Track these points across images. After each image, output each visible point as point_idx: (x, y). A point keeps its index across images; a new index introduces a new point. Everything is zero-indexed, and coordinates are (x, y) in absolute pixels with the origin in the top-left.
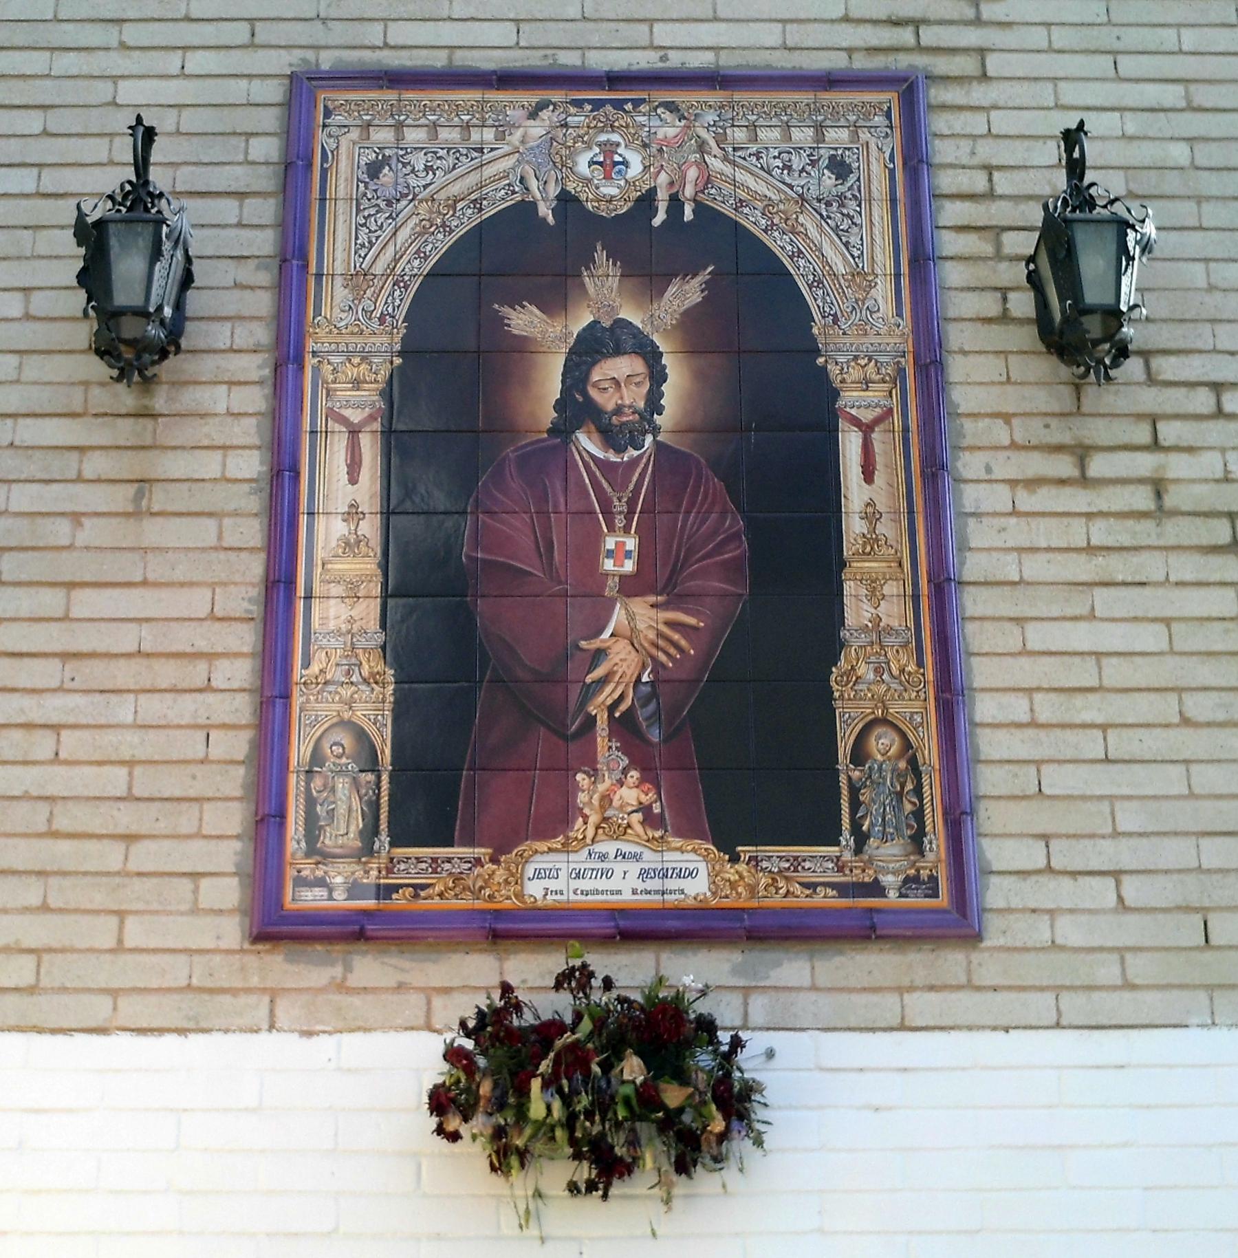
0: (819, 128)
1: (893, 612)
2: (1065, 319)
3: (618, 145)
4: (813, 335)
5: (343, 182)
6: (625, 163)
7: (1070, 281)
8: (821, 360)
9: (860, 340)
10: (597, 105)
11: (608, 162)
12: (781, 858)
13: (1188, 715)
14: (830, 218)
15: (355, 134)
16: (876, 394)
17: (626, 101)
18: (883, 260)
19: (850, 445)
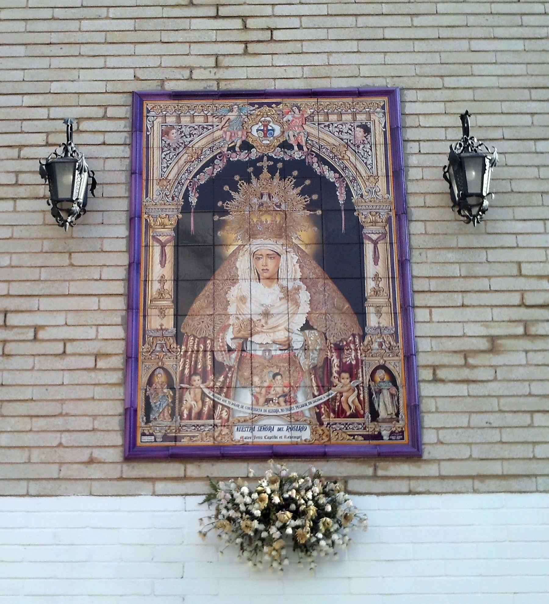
0: (354, 114)
1: (386, 321)
2: (460, 199)
3: (269, 122)
4: (353, 203)
5: (156, 140)
6: (273, 130)
7: (463, 184)
8: (356, 214)
9: (370, 193)
10: (261, 105)
11: (265, 129)
12: (340, 423)
13: (489, 260)
14: (358, 152)
15: (160, 120)
16: (378, 228)
17: (273, 103)
18: (382, 171)
19: (369, 248)
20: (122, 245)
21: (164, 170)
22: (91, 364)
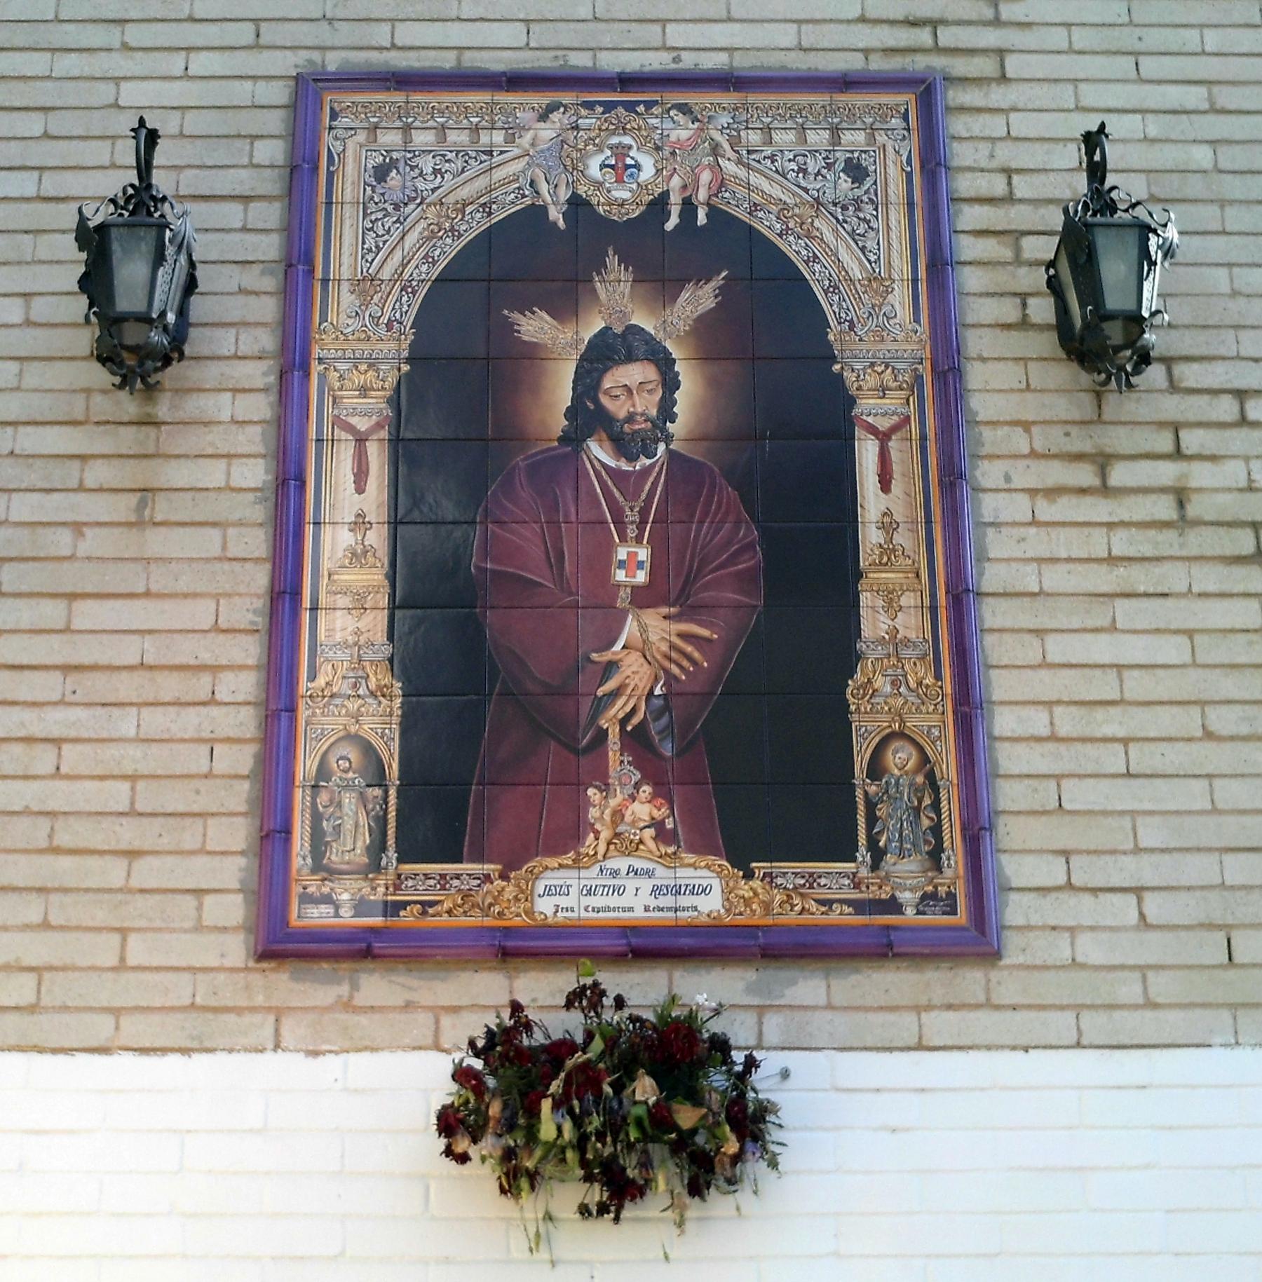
0: (835, 131)
1: (910, 624)
2: (1086, 325)
3: (630, 147)
4: (828, 341)
5: (349, 186)
6: (637, 166)
7: (1091, 287)
8: (837, 367)
9: (876, 346)
10: (609, 107)
11: (620, 165)
12: (796, 874)
14: (846, 222)
16: (893, 402)
17: (638, 103)
18: (900, 265)
19: (867, 453)
22: (249, 38)
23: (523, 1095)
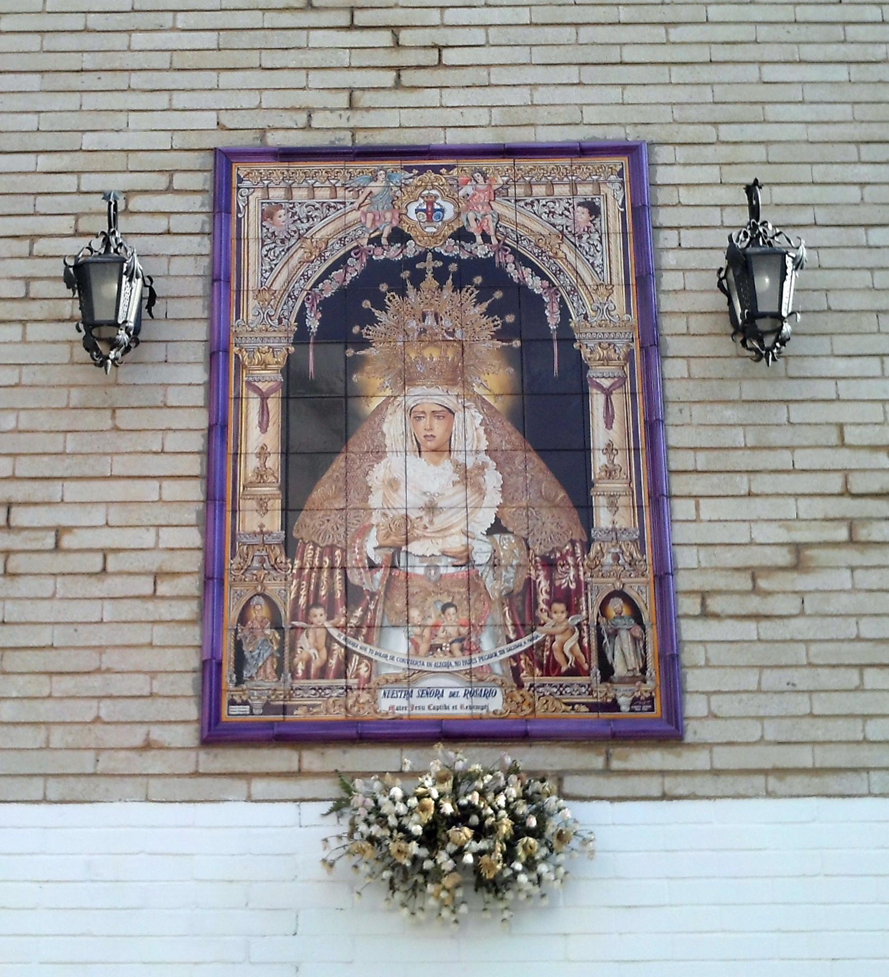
0: (573, 185)
1: (625, 519)
2: (744, 322)
3: (436, 197)
4: (571, 328)
5: (252, 227)
6: (442, 210)
7: (750, 298)
8: (576, 346)
9: (600, 313)
10: (422, 170)
11: (430, 209)
12: (550, 685)
13: (791, 421)
14: (580, 246)
15: (258, 194)
16: (612, 369)
17: (442, 167)
18: (618, 277)
19: (597, 402)
20: (198, 396)
21: (266, 275)
23: (486, 266)
